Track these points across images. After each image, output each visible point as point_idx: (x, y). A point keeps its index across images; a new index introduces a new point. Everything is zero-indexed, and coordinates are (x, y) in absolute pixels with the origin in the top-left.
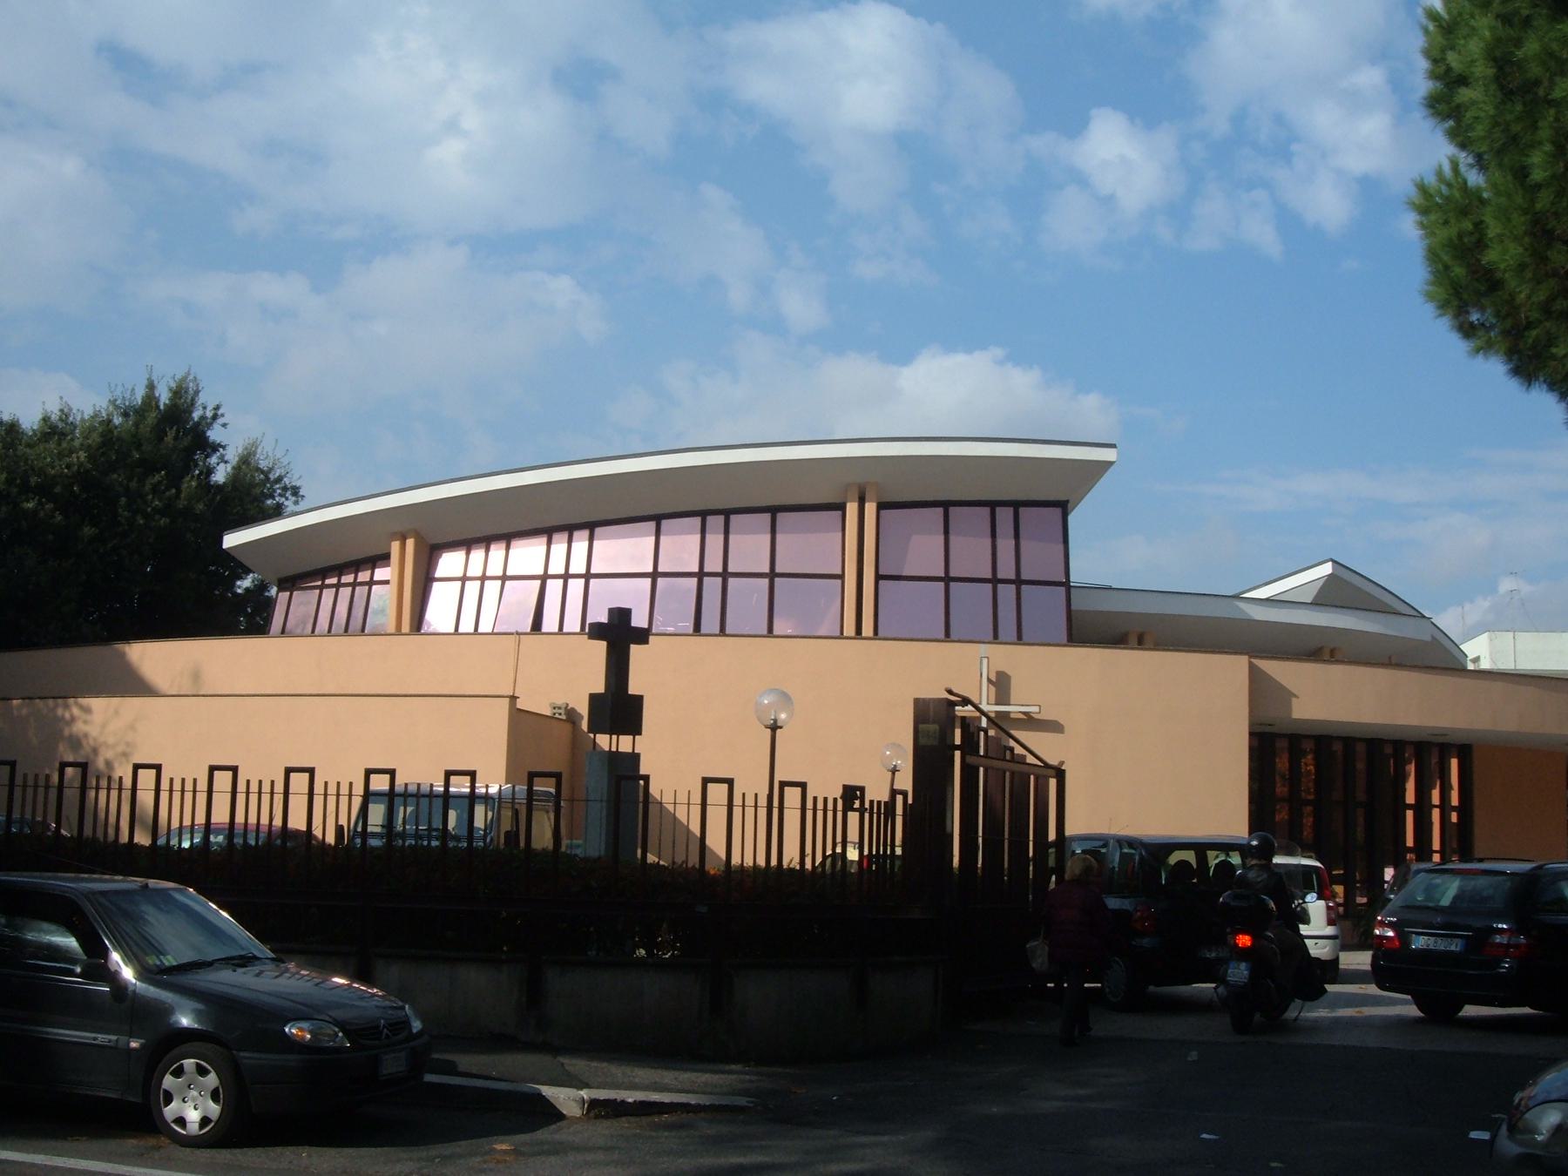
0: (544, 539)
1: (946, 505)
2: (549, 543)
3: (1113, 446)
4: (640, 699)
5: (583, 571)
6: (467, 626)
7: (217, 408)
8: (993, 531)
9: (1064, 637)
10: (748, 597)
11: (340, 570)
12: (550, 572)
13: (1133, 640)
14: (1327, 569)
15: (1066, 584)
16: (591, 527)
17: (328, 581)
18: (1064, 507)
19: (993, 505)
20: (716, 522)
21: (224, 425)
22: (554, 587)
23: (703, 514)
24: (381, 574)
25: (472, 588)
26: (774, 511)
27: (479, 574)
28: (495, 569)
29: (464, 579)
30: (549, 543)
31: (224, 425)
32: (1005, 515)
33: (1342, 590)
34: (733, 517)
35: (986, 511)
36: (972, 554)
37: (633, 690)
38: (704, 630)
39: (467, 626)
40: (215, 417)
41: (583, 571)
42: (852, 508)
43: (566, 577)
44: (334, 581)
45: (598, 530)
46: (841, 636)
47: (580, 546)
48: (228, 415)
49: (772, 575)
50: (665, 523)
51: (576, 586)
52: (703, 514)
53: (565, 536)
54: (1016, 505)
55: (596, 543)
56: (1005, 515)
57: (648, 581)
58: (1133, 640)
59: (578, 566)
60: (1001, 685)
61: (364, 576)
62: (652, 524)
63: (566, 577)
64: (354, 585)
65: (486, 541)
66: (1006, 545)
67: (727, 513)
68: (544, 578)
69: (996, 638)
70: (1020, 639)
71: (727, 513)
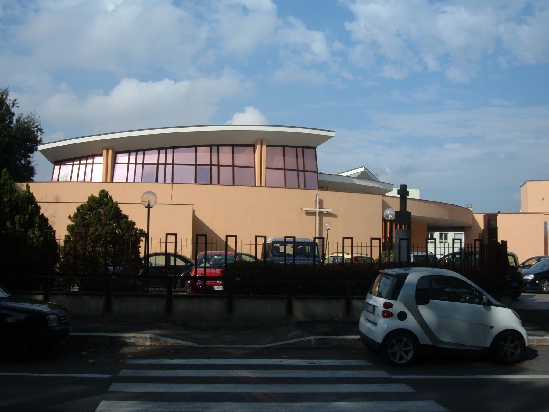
0: (128, 154)
1: (284, 147)
2: (129, 156)
3: (334, 132)
4: (504, 243)
5: (130, 165)
6: (74, 178)
7: (15, 100)
8: (296, 157)
9: (317, 188)
10: (226, 173)
11: (80, 159)
12: (85, 166)
13: (325, 188)
14: (362, 169)
15: (317, 172)
16: (144, 151)
17: (75, 163)
18: (315, 148)
19: (296, 147)
20: (215, 149)
21: (17, 107)
22: (162, 168)
23: (211, 146)
24: (98, 160)
25: (132, 167)
26: (233, 146)
27: (74, 166)
28: (140, 161)
29: (129, 164)
30: (129, 156)
31: (17, 107)
32: (300, 150)
33: (365, 175)
34: (198, 148)
35: (294, 149)
36: (291, 162)
37: (500, 238)
38: (159, 182)
39: (74, 178)
40: (14, 104)
41: (130, 165)
42: (258, 147)
43: (165, 164)
44: (78, 162)
45: (146, 152)
46: (255, 186)
47: (170, 155)
48: (20, 102)
49: (233, 166)
50: (176, 150)
51: (169, 168)
52: (211, 146)
53: (135, 153)
54: (303, 148)
55: (145, 156)
56: (300, 150)
57: (194, 167)
58: (325, 188)
59: (169, 161)
60: (321, 203)
61: (90, 161)
62: (157, 151)
63: (165, 164)
64: (93, 164)
65: (136, 151)
66: (300, 160)
67: (218, 146)
68: (158, 164)
69: (299, 188)
70: (305, 188)
71: (218, 146)
